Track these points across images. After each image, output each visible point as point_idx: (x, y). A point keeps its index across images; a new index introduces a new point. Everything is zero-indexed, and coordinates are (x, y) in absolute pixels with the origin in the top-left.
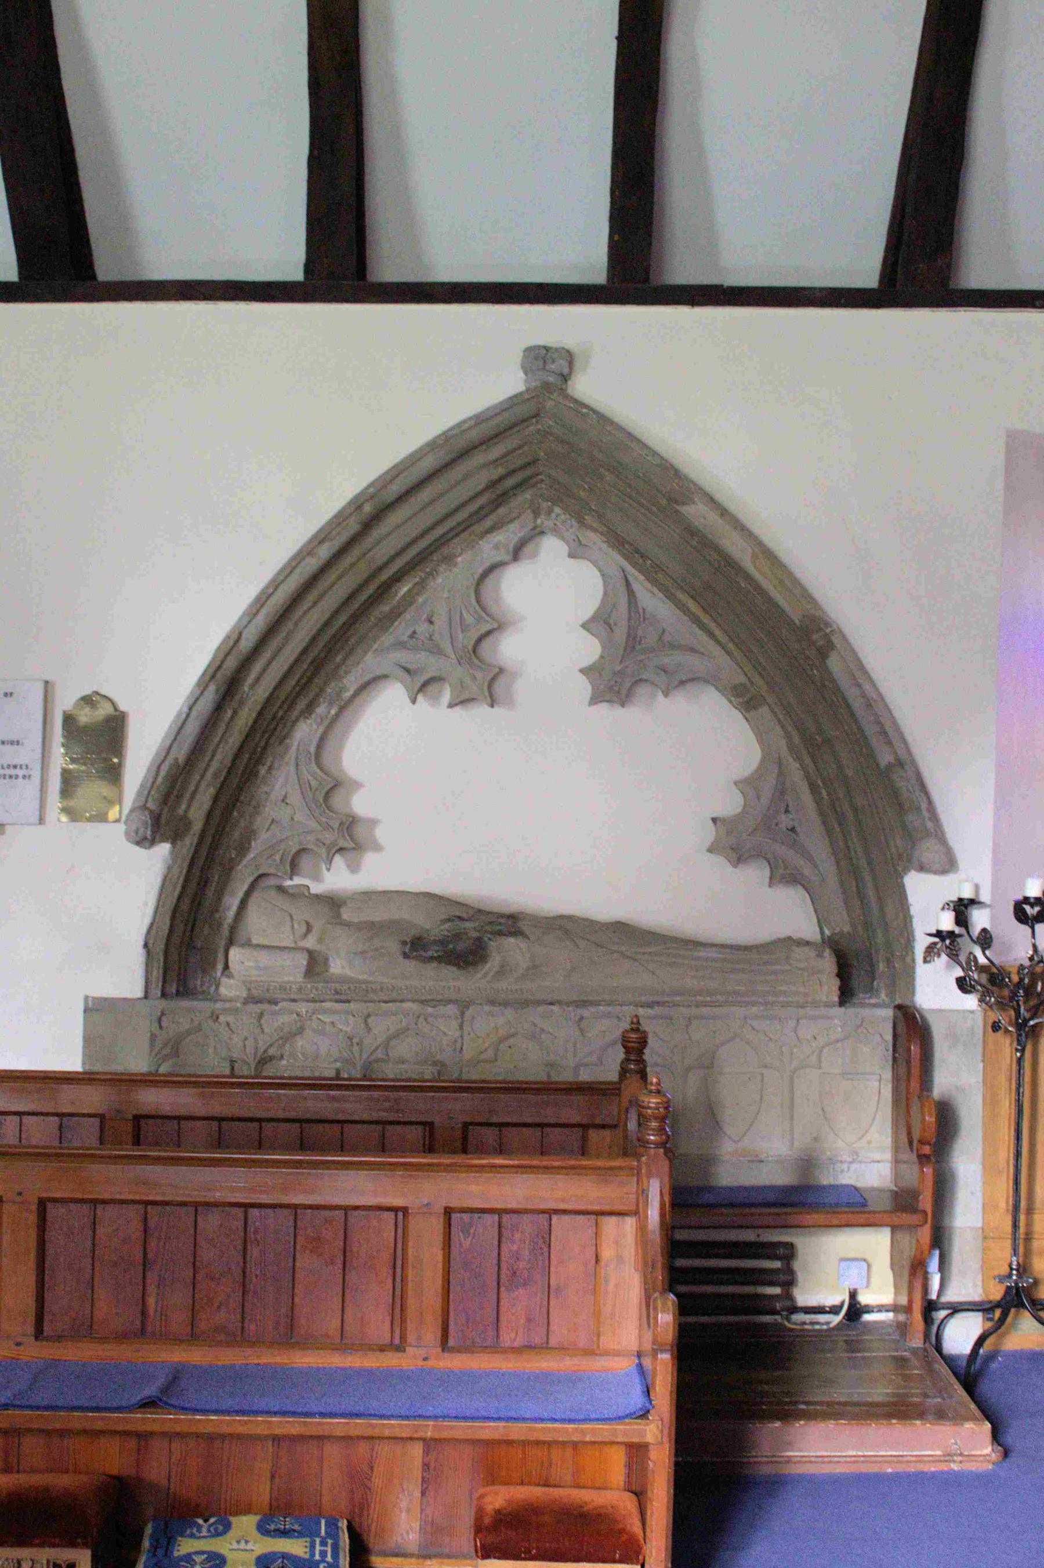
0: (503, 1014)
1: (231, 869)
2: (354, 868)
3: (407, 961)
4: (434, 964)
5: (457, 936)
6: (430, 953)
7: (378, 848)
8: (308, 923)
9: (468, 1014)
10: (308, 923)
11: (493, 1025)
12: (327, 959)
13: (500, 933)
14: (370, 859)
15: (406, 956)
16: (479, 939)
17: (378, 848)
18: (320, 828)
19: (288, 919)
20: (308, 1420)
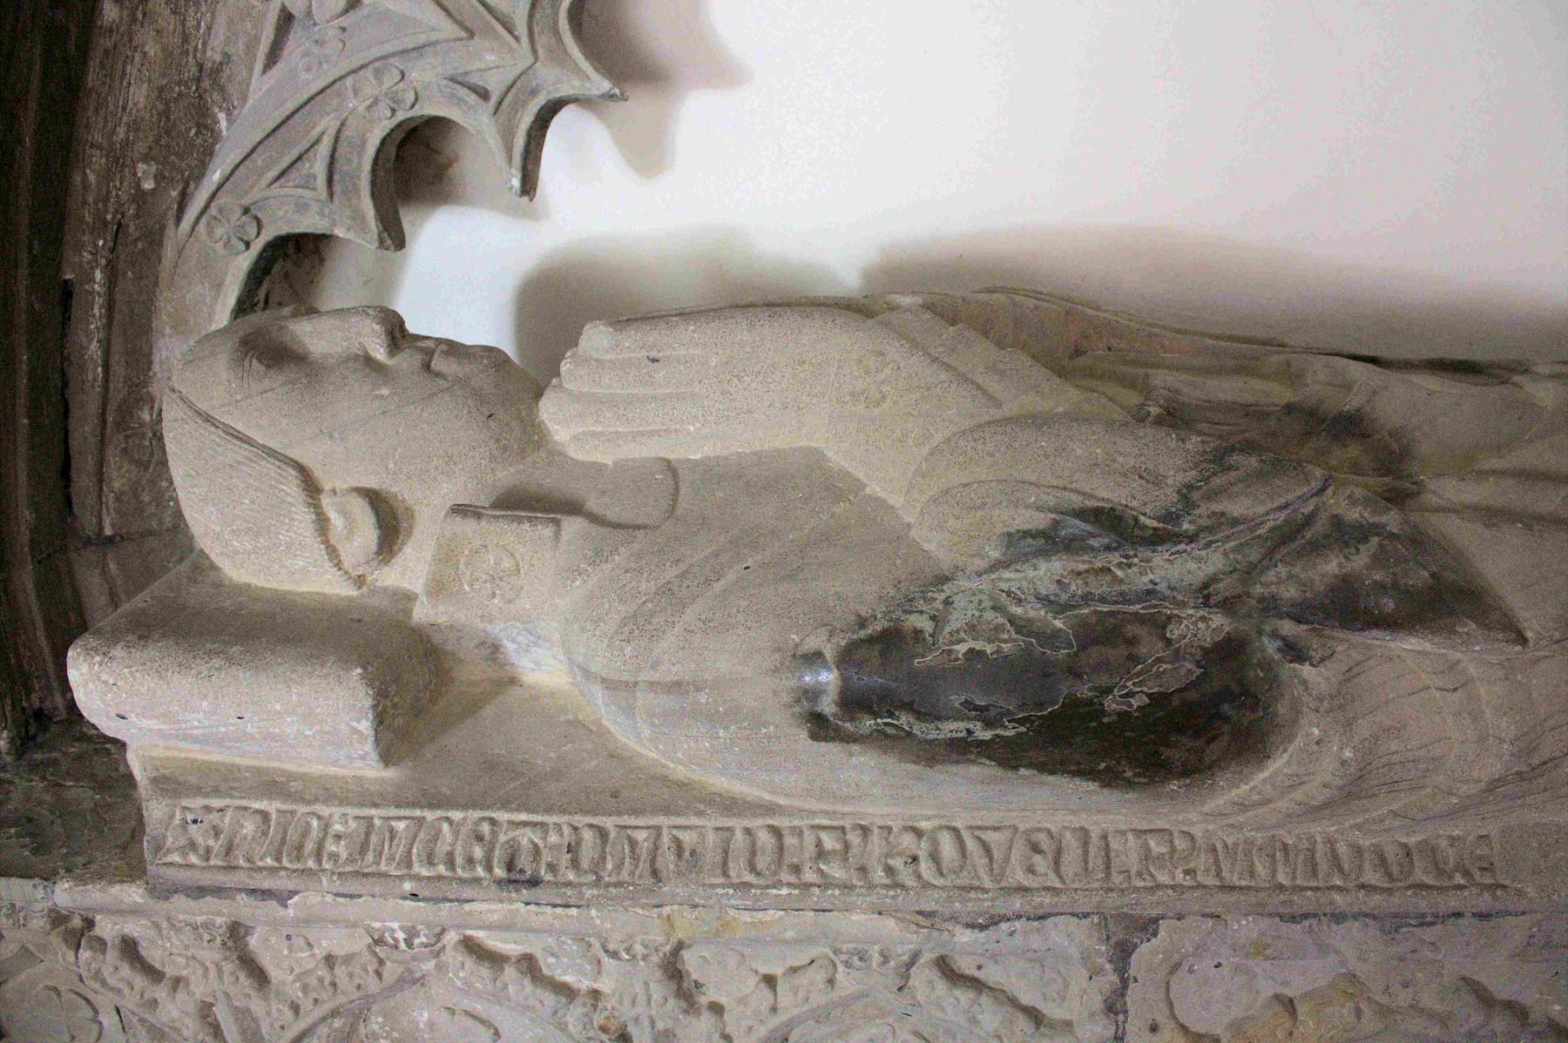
0: (1323, 949)
1: (154, 240)
2: (647, 155)
3: (832, 750)
4: (985, 769)
5: (1110, 632)
6: (952, 728)
7: (723, 72)
8: (377, 500)
9: (1146, 954)
10: (377, 500)
11: (1267, 989)
12: (496, 648)
13: (1347, 609)
14: (697, 115)
15: (820, 727)
16: (1229, 651)
17: (723, 72)
18: (448, 29)
19: (292, 488)
20: (768, 797)
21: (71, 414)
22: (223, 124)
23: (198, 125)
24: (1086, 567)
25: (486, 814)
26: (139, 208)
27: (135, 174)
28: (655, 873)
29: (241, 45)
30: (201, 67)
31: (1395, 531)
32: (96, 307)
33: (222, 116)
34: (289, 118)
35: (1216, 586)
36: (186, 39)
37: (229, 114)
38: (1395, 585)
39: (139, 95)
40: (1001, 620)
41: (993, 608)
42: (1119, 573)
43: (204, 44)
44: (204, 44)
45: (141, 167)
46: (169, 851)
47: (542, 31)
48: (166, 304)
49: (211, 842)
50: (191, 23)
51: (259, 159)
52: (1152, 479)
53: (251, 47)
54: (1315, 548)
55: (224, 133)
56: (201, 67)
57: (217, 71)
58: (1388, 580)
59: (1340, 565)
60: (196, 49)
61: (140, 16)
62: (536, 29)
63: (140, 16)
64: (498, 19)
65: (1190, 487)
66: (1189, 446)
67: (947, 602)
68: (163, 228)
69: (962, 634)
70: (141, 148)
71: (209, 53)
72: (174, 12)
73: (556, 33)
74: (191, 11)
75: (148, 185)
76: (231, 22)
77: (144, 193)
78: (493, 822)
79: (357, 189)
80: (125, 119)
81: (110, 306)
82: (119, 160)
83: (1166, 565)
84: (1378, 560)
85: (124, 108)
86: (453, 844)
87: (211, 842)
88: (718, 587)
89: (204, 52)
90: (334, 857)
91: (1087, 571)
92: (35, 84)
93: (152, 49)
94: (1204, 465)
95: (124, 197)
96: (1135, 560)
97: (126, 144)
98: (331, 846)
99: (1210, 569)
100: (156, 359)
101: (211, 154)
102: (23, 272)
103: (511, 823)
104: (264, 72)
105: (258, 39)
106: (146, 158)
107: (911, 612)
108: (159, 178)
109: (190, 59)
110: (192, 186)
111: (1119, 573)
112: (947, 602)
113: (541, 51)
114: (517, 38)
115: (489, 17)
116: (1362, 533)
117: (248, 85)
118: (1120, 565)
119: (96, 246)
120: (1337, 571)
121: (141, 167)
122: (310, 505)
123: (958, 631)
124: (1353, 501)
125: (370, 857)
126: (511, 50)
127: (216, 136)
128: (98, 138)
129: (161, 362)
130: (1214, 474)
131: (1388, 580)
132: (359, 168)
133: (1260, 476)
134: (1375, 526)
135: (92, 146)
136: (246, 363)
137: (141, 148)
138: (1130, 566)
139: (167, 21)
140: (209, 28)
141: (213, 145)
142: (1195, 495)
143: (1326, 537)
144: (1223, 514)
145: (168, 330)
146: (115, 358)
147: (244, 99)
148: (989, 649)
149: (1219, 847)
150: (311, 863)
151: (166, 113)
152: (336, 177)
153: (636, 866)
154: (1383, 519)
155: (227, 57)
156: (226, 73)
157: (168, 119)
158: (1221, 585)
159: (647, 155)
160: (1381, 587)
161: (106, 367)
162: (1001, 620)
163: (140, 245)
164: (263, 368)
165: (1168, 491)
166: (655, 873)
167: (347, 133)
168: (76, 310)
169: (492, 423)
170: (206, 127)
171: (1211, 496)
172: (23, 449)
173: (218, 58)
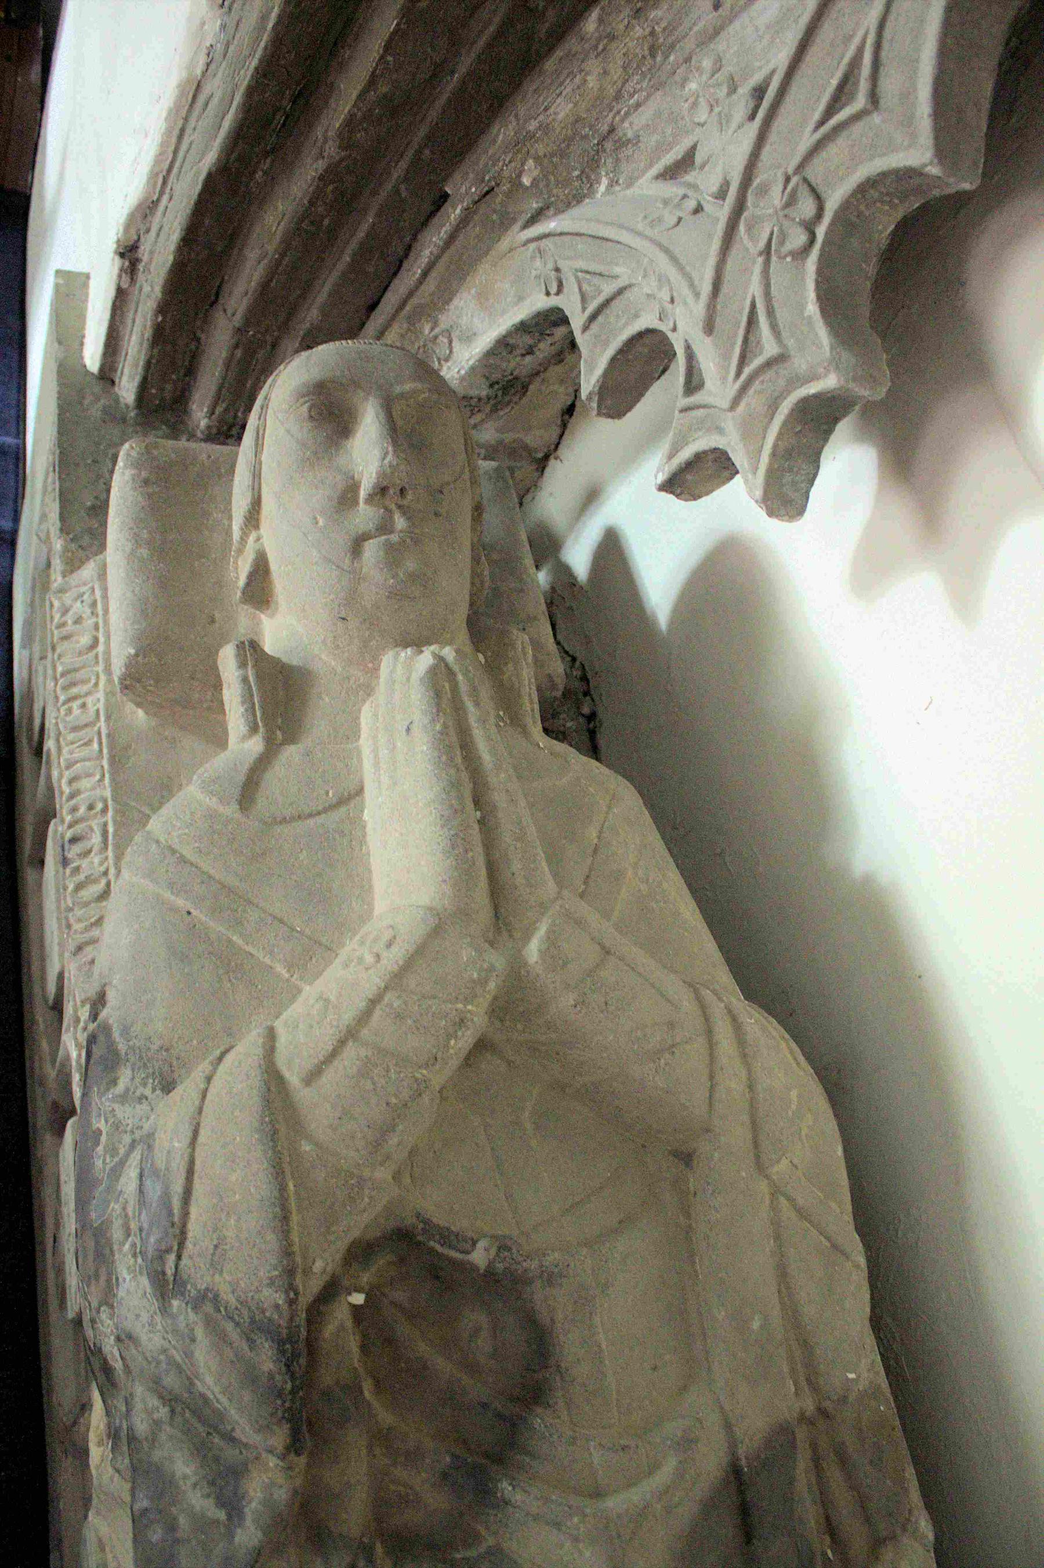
1: (505, 223)
2: (871, 570)
7: (964, 594)
17: (964, 594)
21: (399, 276)
22: (602, 188)
23: (582, 172)
24: (130, 1214)
25: (110, 802)
26: (510, 191)
27: (523, 164)
28: (80, 948)
29: (655, 138)
30: (612, 130)
31: (237, 1539)
32: (444, 229)
33: (605, 182)
34: (607, 240)
35: (132, 1347)
36: (618, 97)
37: (610, 185)
38: (177, 1541)
39: (562, 110)
40: (122, 1151)
41: (134, 1141)
42: (127, 1246)
43: (627, 114)
44: (627, 114)
45: (530, 163)
46: (60, 599)
47: (760, 392)
48: (482, 274)
49: (70, 622)
50: (629, 87)
51: (581, 245)
52: (217, 1260)
53: (661, 149)
54: (201, 1450)
55: (599, 196)
56: (612, 130)
57: (622, 144)
58: (179, 1534)
59: (185, 1477)
60: (619, 112)
61: (601, 47)
62: (756, 385)
63: (601, 47)
64: (746, 340)
65: (216, 1297)
66: (266, 1292)
67: (143, 1098)
68: (514, 220)
69: (111, 1121)
70: (541, 149)
71: (626, 125)
72: (624, 68)
73: (773, 408)
74: (637, 78)
75: (526, 181)
76: (658, 114)
77: (520, 184)
78: (105, 810)
79: (606, 343)
80: (541, 118)
81: (452, 238)
82: (520, 144)
83: (140, 1292)
84: (202, 1524)
85: (546, 109)
86: (86, 790)
87: (70, 622)
88: (167, 895)
89: (622, 121)
90: (70, 711)
91: (126, 1216)
92: (481, 43)
93: (592, 82)
94: (245, 1313)
95: (506, 173)
96: (140, 1260)
97: (531, 136)
98: (75, 705)
99: (144, 1338)
100: (456, 302)
101: (579, 202)
102: (403, 164)
103: (105, 825)
104: (657, 178)
105: (670, 146)
106: (537, 159)
107: (133, 1070)
108: (535, 182)
109: (611, 115)
110: (552, 211)
111: (127, 1246)
112: (143, 1098)
113: (741, 408)
114: (738, 374)
115: (741, 332)
116: (232, 1505)
117: (638, 178)
118: (134, 1245)
119: (470, 188)
120: (178, 1474)
121: (530, 163)
122: (242, 529)
123: (114, 1116)
124: (268, 1487)
125: (71, 737)
126: (724, 379)
127: (591, 192)
128: (522, 113)
129: (457, 308)
130: (237, 1324)
131: (179, 1534)
132: (622, 329)
133: (250, 1377)
134: (241, 1516)
135: (516, 116)
136: (302, 400)
137: (541, 149)
138: (135, 1255)
139: (616, 73)
140: (638, 105)
141: (585, 196)
142: (208, 1307)
143: (217, 1459)
144: (193, 1340)
145: (473, 291)
146: (434, 274)
147: (629, 185)
148: (100, 1149)
149: (123, 1434)
150: (62, 698)
151: (569, 140)
152: (600, 319)
153: (82, 933)
154: (249, 1522)
155: (637, 140)
156: (629, 151)
157: (568, 146)
158: (134, 1351)
159: (871, 570)
160: (172, 1527)
161: (425, 274)
162: (122, 1151)
163: (495, 217)
164: (306, 415)
165: (209, 1279)
166: (80, 948)
167: (627, 294)
168: (435, 220)
169: (340, 624)
170: (588, 177)
171: (209, 1323)
172: (335, 275)
173: (630, 134)
